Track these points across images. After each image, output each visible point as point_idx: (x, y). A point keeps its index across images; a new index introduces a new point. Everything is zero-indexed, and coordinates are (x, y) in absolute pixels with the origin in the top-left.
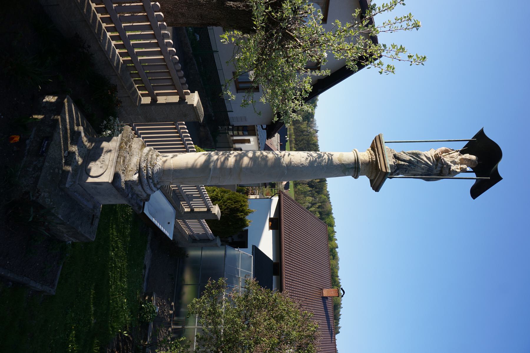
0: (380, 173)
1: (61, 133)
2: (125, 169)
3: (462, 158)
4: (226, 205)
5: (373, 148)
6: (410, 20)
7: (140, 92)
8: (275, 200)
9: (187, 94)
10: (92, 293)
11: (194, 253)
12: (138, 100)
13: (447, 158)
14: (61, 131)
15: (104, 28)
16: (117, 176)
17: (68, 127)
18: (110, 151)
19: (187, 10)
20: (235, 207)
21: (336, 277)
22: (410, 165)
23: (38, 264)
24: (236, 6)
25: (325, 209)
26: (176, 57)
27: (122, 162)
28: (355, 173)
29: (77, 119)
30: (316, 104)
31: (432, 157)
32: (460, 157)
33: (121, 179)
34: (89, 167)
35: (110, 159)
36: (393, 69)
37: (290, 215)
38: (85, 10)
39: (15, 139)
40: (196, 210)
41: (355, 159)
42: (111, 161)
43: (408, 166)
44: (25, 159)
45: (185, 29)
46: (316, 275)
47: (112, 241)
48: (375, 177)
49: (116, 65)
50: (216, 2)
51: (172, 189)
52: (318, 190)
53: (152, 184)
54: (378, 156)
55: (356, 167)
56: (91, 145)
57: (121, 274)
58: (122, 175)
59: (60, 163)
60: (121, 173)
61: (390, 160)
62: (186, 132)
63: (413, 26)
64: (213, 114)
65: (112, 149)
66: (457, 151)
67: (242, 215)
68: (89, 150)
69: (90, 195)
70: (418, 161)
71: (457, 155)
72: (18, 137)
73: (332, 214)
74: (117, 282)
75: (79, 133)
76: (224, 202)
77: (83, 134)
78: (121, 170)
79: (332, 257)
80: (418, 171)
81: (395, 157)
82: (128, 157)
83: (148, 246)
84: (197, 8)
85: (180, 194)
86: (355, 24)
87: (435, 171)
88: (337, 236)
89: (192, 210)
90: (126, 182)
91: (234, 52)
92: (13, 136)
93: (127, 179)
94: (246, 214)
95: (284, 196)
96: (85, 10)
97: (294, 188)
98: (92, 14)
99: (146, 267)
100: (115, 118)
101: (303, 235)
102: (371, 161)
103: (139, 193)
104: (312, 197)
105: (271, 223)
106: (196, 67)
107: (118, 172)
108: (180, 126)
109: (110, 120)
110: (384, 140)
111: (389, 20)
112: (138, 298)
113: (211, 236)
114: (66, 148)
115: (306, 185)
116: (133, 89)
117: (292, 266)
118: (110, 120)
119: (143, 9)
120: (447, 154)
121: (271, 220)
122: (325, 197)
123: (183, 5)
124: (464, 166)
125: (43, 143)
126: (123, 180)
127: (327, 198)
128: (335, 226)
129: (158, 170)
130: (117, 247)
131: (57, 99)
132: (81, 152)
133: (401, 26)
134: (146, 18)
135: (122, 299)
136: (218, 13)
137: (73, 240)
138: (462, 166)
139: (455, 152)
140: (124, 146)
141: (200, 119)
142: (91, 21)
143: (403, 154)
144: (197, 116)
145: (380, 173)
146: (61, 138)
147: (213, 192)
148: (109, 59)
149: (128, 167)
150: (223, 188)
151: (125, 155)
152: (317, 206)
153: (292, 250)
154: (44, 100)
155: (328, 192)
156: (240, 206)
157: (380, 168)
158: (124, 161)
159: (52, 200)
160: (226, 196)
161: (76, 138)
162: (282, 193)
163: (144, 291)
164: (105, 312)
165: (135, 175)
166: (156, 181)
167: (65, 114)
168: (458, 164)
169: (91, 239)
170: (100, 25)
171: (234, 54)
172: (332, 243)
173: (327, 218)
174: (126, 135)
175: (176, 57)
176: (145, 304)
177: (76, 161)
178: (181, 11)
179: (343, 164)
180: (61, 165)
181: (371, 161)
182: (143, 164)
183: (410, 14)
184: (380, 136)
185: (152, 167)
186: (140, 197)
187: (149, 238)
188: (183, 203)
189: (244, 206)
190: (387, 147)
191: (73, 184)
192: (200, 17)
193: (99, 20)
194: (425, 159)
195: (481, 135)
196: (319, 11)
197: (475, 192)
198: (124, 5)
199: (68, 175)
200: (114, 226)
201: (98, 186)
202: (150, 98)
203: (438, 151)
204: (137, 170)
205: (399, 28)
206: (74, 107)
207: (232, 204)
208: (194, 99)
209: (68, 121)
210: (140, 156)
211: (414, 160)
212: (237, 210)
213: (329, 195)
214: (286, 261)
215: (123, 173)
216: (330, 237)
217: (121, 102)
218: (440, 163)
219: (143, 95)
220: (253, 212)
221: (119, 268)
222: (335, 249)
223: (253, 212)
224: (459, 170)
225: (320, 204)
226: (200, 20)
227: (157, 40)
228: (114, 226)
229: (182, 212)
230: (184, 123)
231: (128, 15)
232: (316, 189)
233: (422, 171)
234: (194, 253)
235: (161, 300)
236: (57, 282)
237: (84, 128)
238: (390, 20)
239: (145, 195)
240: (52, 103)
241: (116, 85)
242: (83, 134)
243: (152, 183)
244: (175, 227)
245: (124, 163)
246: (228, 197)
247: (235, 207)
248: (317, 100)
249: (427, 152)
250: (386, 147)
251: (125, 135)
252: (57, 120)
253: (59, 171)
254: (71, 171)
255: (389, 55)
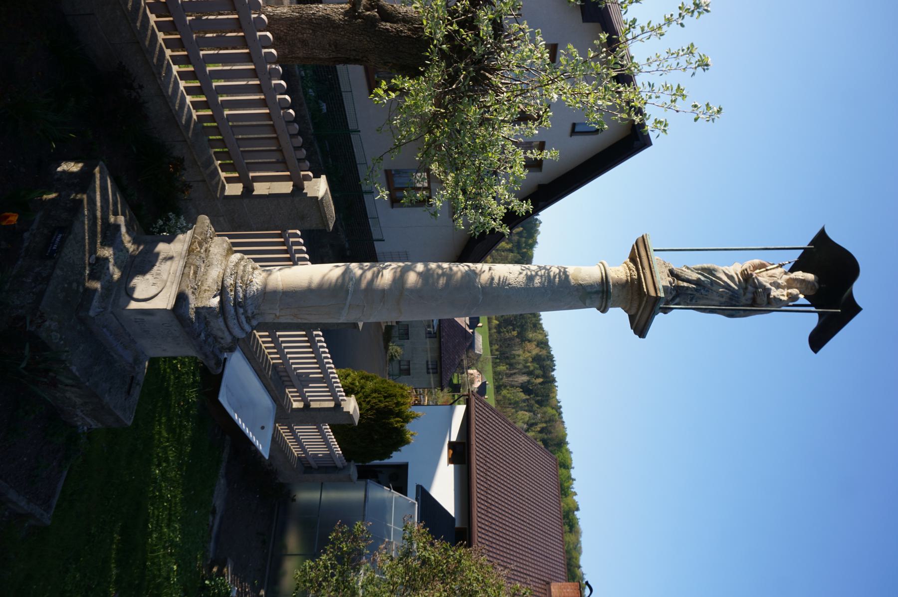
0: (645, 299)
1: (86, 222)
2: (196, 287)
3: (791, 278)
4: (369, 402)
5: (633, 259)
6: (692, 53)
7: (223, 175)
8: (460, 410)
9: (307, 178)
10: (115, 541)
11: (306, 496)
12: (219, 188)
13: (763, 277)
14: (86, 220)
15: (168, 57)
16: (181, 298)
17: (99, 214)
18: (171, 258)
19: (311, 34)
20: (386, 406)
21: (576, 567)
22: (699, 288)
23: (25, 459)
24: (395, 29)
25: (554, 435)
26: (291, 111)
27: (191, 275)
28: (603, 301)
29: (115, 204)
30: (536, 239)
31: (737, 275)
32: (786, 277)
33: (188, 303)
34: (132, 284)
35: (170, 270)
36: (665, 126)
37: (488, 437)
38: (138, 24)
39: (10, 219)
40: (314, 405)
41: (602, 273)
42: (171, 273)
43: (696, 290)
44: (19, 263)
45: (301, 91)
46: (538, 555)
47: (158, 447)
48: (638, 309)
49: (185, 122)
50: (362, 22)
51: (272, 362)
52: (539, 398)
53: (243, 316)
54: (641, 271)
55: (603, 292)
56: (138, 249)
57: (170, 514)
58: (191, 298)
59: (82, 273)
60: (189, 292)
61: (663, 277)
62: (301, 251)
63: (697, 65)
64: (347, 246)
65: (175, 255)
66: (780, 265)
67: (398, 422)
68: (133, 257)
69: (130, 336)
70: (713, 283)
71: (781, 273)
72: (16, 216)
73: (567, 443)
74: (161, 527)
75: (118, 227)
76: (366, 397)
77: (123, 229)
78: (189, 288)
79: (567, 528)
80: (712, 300)
81: (672, 273)
82: (203, 268)
83: (222, 471)
84: (330, 32)
85: (285, 374)
86: (602, 53)
87: (743, 300)
88: (576, 487)
89: (307, 406)
90: (198, 310)
91: (391, 110)
92: (7, 214)
93: (200, 305)
94: (406, 419)
95: (476, 401)
96: (138, 24)
97: (495, 394)
98: (149, 32)
99: (215, 511)
100: (178, 216)
101: (511, 479)
102: (629, 280)
103: (220, 334)
104: (529, 411)
105: (451, 452)
106: (320, 158)
107: (185, 290)
108: (291, 240)
109: (170, 220)
110: (652, 246)
111: (657, 54)
112: (198, 567)
113: (341, 461)
114: (93, 251)
115: (518, 389)
116: (212, 167)
117: (490, 534)
118: (170, 220)
119: (237, 25)
120: (764, 271)
121: (451, 445)
122: (554, 412)
123: (305, 26)
124: (795, 291)
125: (54, 237)
126: (192, 306)
127: (557, 414)
128: (573, 468)
129: (254, 293)
130: (167, 460)
131: (82, 168)
132: (118, 258)
133: (678, 64)
134: (243, 42)
135: (169, 562)
136: (365, 40)
137: (92, 423)
138: (790, 291)
139: (777, 267)
140: (197, 248)
141: (328, 224)
142: (147, 43)
143: (686, 270)
144: (323, 218)
145: (645, 299)
146: (86, 231)
147: (346, 379)
148: (174, 111)
149: (202, 284)
150: (364, 372)
151: (198, 263)
152: (539, 429)
153: (491, 504)
154: (59, 169)
155: (559, 402)
156: (394, 406)
157: (645, 290)
158: (195, 273)
159: (64, 337)
160: (370, 385)
161: (111, 235)
162: (473, 395)
163: (211, 555)
164: (137, 582)
165: (213, 297)
166: (250, 312)
167: (95, 192)
168: (783, 288)
169: (126, 421)
170: (162, 52)
171: (391, 113)
172: (568, 500)
173: (556, 451)
174: (201, 230)
175: (291, 111)
176: (211, 580)
177: (109, 273)
178: (302, 36)
179: (581, 285)
180: (83, 277)
181: (629, 280)
182: (228, 280)
183: (692, 45)
184: (645, 238)
185: (244, 287)
186: (220, 343)
187: (225, 456)
188: (290, 392)
189: (403, 404)
190: (656, 257)
191: (102, 312)
192: (333, 47)
193: (161, 44)
194: (725, 279)
195: (822, 238)
196: (538, 32)
197: (817, 340)
198: (206, 17)
199: (94, 295)
200: (164, 420)
201: (146, 318)
202: (240, 186)
203: (747, 265)
204: (218, 290)
205: (674, 66)
206: (111, 182)
207: (380, 401)
208: (319, 187)
209: (99, 204)
210: (223, 267)
211: (706, 279)
212: (387, 413)
213: (560, 407)
214: (479, 525)
215: (193, 293)
216: (564, 489)
217: (190, 187)
218: (751, 285)
219: (229, 180)
220: (419, 417)
221: (168, 501)
222: (574, 512)
223: (419, 417)
224: (785, 298)
225: (544, 425)
226: (333, 52)
227: (260, 80)
228: (164, 420)
229: (288, 409)
230: (299, 232)
231: (210, 35)
232: (537, 396)
233: (721, 299)
234: (306, 496)
235: (241, 583)
236: (55, 502)
237: (126, 221)
238: (658, 54)
239: (229, 339)
240: (72, 173)
241: (184, 157)
242: (123, 229)
243: (243, 314)
244: (274, 440)
245: (196, 277)
246: (374, 388)
247: (384, 408)
248: (541, 324)
249: (727, 267)
250: (655, 257)
251: (198, 230)
252: (81, 201)
253: (78, 286)
254: (100, 290)
255: (660, 102)
